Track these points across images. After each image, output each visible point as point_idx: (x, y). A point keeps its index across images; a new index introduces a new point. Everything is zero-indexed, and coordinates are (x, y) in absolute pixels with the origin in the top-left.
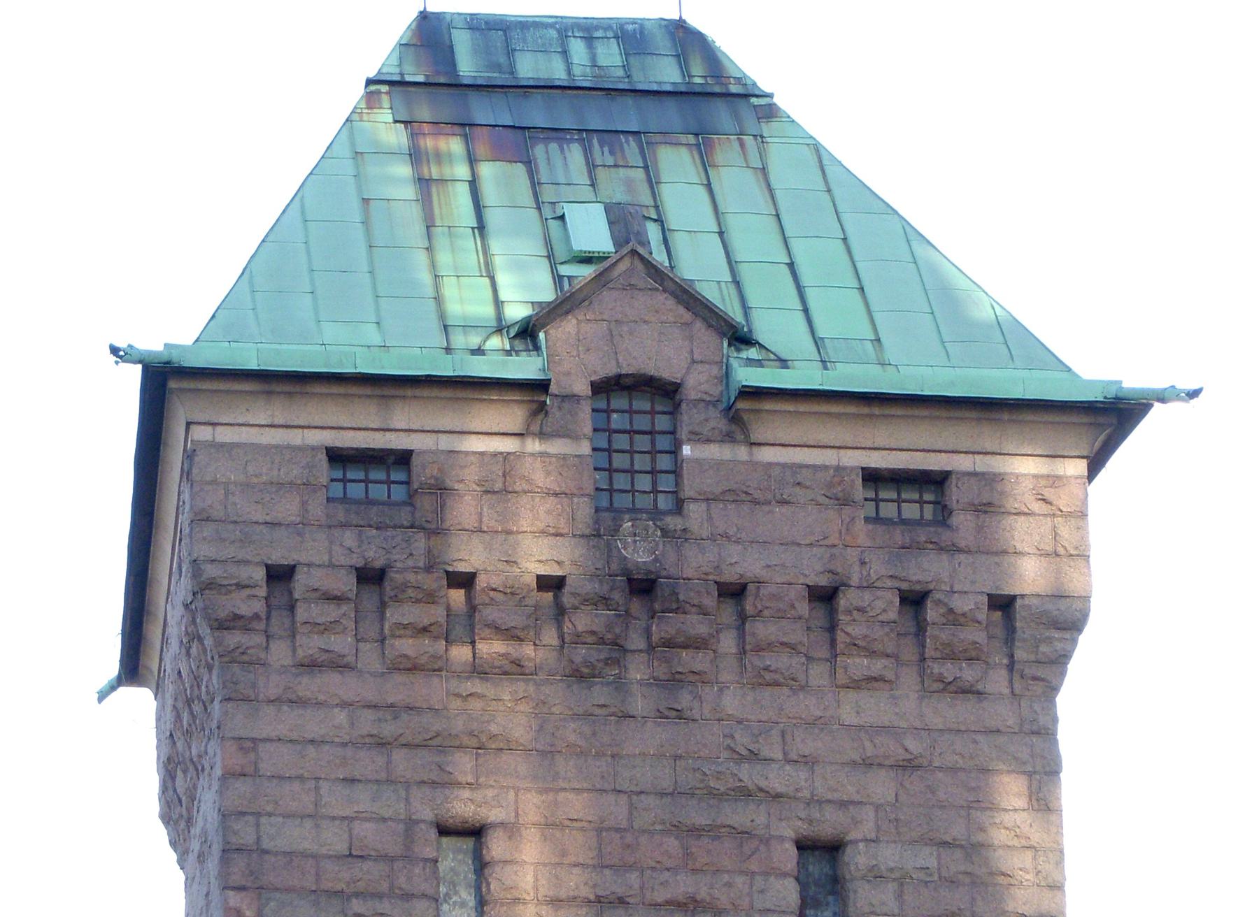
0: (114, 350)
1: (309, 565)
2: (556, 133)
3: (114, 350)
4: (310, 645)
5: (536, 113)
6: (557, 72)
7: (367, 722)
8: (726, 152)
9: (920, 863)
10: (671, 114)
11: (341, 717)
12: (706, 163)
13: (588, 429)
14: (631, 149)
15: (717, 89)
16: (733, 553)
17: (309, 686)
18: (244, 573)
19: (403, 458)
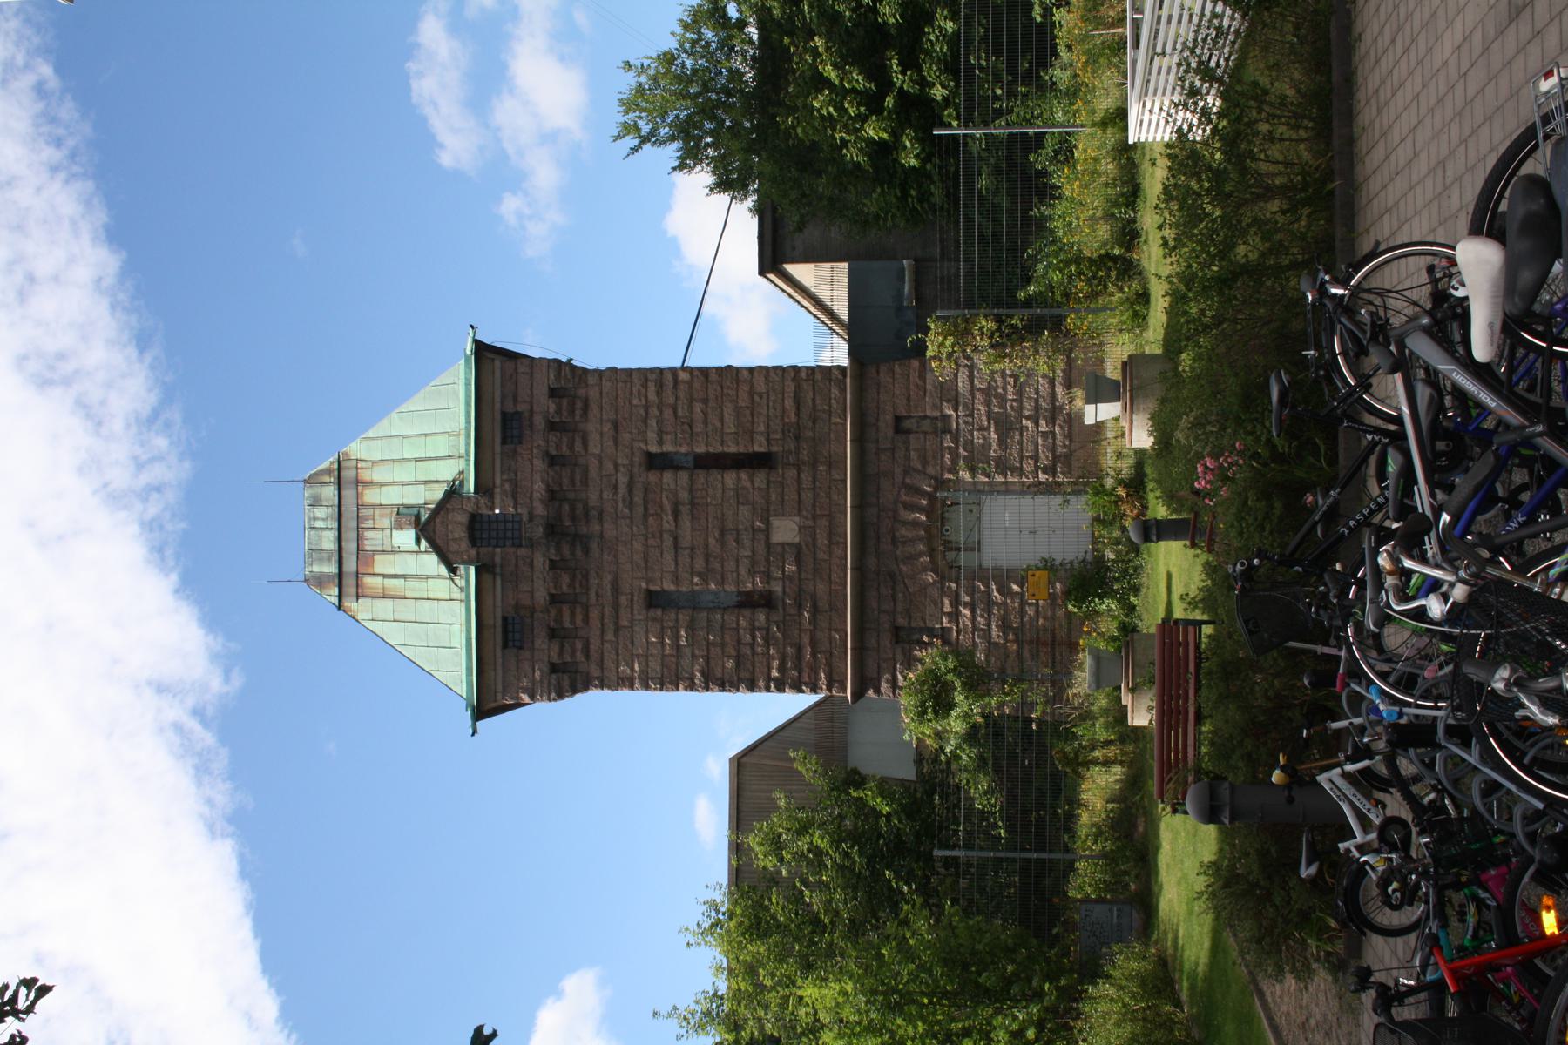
0: (473, 735)
1: (549, 657)
2: (359, 539)
3: (473, 735)
4: (579, 656)
5: (350, 547)
6: (332, 535)
7: (610, 636)
8: (365, 475)
9: (655, 424)
10: (348, 494)
11: (607, 646)
12: (370, 484)
13: (490, 549)
14: (363, 512)
15: (336, 473)
16: (536, 495)
17: (594, 655)
18: (553, 682)
19: (505, 619)
